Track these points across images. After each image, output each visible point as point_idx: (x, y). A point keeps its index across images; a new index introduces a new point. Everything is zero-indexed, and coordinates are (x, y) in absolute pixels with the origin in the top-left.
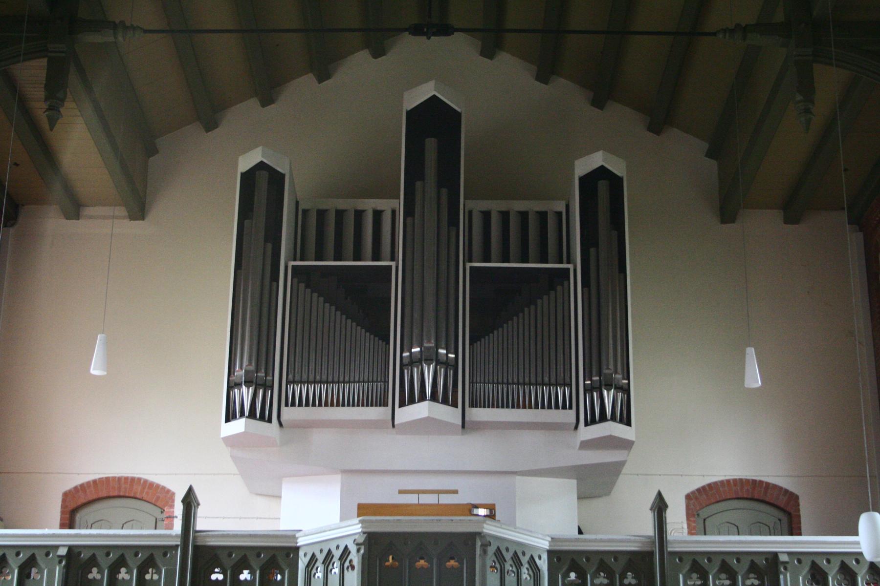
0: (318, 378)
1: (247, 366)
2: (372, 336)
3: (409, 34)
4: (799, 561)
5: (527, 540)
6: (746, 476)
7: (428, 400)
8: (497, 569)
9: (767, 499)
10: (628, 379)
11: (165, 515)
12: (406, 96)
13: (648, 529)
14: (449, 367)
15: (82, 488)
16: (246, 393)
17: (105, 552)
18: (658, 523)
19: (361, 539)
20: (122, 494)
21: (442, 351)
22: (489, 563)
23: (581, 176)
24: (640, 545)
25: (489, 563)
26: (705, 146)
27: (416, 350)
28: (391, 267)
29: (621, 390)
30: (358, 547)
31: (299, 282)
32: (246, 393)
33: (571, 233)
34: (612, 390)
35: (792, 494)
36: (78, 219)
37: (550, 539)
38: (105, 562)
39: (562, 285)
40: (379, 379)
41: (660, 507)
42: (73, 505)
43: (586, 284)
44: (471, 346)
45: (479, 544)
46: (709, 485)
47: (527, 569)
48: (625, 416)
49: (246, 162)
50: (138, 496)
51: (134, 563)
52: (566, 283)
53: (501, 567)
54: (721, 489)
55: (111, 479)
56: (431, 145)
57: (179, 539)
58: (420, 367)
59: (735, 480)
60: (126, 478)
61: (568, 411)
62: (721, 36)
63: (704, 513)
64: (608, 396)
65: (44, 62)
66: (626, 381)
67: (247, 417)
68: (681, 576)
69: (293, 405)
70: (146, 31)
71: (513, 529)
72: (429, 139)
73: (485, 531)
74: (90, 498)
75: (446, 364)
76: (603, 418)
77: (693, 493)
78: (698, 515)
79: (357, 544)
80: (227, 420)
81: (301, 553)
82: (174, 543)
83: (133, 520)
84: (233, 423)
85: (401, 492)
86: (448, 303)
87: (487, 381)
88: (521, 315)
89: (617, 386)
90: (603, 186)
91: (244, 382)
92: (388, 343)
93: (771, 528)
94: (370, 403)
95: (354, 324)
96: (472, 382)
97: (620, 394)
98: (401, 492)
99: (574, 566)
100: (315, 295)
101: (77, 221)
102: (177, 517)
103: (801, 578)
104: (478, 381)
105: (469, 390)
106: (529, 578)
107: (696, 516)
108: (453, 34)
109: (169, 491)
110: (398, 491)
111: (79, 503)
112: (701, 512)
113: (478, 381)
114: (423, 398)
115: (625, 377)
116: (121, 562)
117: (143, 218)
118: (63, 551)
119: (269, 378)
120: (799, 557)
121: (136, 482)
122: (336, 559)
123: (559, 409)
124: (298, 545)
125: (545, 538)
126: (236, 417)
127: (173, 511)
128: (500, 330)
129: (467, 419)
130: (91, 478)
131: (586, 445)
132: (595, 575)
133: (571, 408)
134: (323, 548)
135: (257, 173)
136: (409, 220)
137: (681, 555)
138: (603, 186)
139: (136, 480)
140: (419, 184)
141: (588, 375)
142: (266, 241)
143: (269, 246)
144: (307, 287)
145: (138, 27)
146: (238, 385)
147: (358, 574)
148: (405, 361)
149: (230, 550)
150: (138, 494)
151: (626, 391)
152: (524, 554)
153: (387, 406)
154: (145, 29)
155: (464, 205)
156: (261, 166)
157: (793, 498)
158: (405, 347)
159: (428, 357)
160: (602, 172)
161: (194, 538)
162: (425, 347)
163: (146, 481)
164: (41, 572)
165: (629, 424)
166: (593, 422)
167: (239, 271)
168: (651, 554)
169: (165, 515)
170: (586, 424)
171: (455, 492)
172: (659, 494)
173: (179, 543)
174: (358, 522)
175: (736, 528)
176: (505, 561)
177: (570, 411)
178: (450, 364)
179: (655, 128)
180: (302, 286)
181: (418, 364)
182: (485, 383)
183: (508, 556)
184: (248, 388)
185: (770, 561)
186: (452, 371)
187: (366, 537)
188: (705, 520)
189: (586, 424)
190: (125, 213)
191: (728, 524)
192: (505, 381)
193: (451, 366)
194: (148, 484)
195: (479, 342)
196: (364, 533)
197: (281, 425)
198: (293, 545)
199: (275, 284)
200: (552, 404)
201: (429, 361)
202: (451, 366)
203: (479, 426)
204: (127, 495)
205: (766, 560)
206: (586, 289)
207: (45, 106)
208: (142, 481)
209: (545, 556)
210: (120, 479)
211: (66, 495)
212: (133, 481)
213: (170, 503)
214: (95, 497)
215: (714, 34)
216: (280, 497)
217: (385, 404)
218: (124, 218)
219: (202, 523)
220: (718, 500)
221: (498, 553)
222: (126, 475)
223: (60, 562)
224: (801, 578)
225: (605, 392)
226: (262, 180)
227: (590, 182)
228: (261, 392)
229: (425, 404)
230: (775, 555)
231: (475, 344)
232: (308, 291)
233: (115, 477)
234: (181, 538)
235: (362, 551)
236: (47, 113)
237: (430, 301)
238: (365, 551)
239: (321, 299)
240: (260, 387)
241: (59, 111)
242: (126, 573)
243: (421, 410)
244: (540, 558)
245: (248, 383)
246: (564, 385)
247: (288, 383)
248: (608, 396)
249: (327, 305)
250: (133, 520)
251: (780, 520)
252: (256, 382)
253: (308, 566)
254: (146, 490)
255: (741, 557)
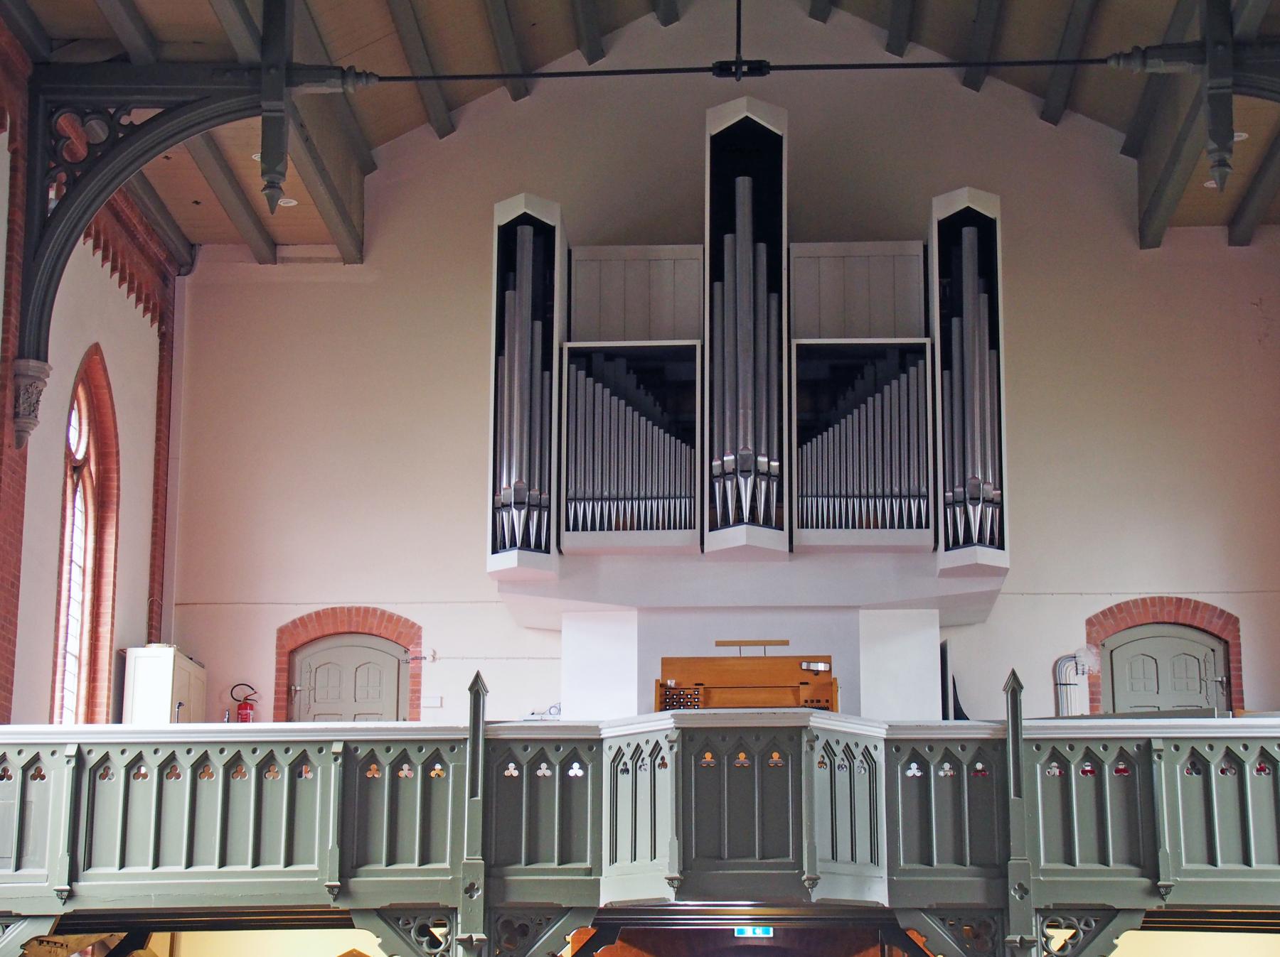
0: (606, 494)
1: (516, 483)
2: (673, 438)
3: (714, 75)
4: (1177, 748)
5: (863, 730)
6: (1168, 593)
7: (746, 523)
8: (826, 765)
9: (1195, 624)
10: (1001, 488)
11: (410, 656)
12: (710, 113)
13: (1001, 712)
14: (772, 478)
15: (302, 622)
16: (518, 516)
17: (385, 747)
18: (1012, 708)
19: (675, 735)
20: (353, 630)
21: (763, 460)
22: (817, 758)
23: (940, 219)
24: (991, 732)
25: (817, 758)
26: (1119, 138)
27: (729, 458)
28: (694, 346)
29: (990, 504)
30: (671, 744)
31: (577, 370)
32: (518, 516)
33: (930, 280)
34: (980, 506)
35: (1230, 616)
36: (276, 264)
37: (887, 727)
38: (386, 759)
39: (916, 365)
40: (683, 494)
41: (1014, 688)
42: (291, 646)
43: (947, 364)
44: (800, 449)
45: (805, 739)
46: (1118, 606)
47: (861, 761)
48: (997, 536)
49: (505, 213)
50: (374, 633)
51: (418, 758)
52: (921, 362)
53: (831, 762)
54: (1134, 611)
55: (338, 611)
56: (743, 185)
57: (468, 733)
58: (735, 480)
59: (1153, 599)
60: (358, 609)
61: (924, 531)
62: (1112, 63)
63: (1111, 642)
64: (975, 513)
65: (257, 122)
66: (999, 492)
67: (519, 549)
68: (1038, 766)
69: (575, 528)
70: (381, 79)
71: (844, 720)
72: (741, 177)
73: (811, 724)
74: (313, 636)
75: (768, 475)
76: (968, 541)
77: (1096, 616)
78: (1103, 645)
79: (669, 742)
80: (494, 551)
81: (606, 746)
82: (462, 737)
83: (370, 663)
84: (502, 556)
85: (719, 644)
86: (768, 318)
87: (820, 494)
88: (863, 406)
89: (986, 499)
90: (969, 235)
91: (514, 503)
92: (693, 446)
93: (1201, 661)
94: (671, 525)
95: (650, 423)
96: (801, 496)
97: (991, 508)
98: (719, 644)
99: (915, 757)
100: (599, 386)
101: (273, 266)
102: (425, 658)
103: (1178, 767)
104: (809, 494)
105: (798, 484)
106: (863, 772)
107: (1101, 647)
108: (769, 73)
109: (413, 625)
110: (714, 644)
111: (300, 642)
112: (1107, 642)
113: (809, 494)
114: (739, 520)
115: (997, 487)
116: (404, 758)
117: (361, 261)
118: (338, 748)
119: (545, 496)
120: (1176, 743)
121: (371, 613)
122: (646, 754)
123: (913, 528)
124: (602, 737)
125: (881, 726)
126: (504, 547)
127: (421, 651)
128: (837, 426)
129: (795, 543)
130: (312, 609)
131: (946, 573)
132: (939, 766)
133: (927, 526)
134: (631, 742)
135: (518, 228)
136: (717, 285)
137: (1038, 743)
138: (969, 235)
139: (371, 611)
140: (728, 238)
141: (950, 484)
142: (534, 318)
143: (538, 325)
144: (588, 375)
145: (371, 74)
146: (506, 506)
147: (671, 772)
148: (716, 471)
149: (526, 743)
150: (375, 629)
151: (1000, 505)
152: (857, 745)
153: (694, 528)
154: (380, 76)
155: (788, 250)
156: (525, 219)
157: (1232, 621)
158: (716, 456)
159: (744, 468)
160: (968, 216)
161: (485, 731)
162: (740, 455)
163: (383, 612)
164: (314, 770)
165: (1001, 547)
166: (956, 544)
167: (500, 357)
168: (1003, 742)
169: (410, 656)
170: (947, 548)
171: (786, 643)
172: (1014, 673)
173: (468, 736)
174: (670, 716)
175: (1154, 661)
176: (836, 755)
177: (927, 530)
178: (773, 474)
179: (1052, 116)
180: (582, 373)
181: (732, 475)
182: (817, 496)
183: (838, 750)
184: (520, 511)
185: (1142, 748)
186: (775, 484)
187: (679, 734)
188: (1112, 651)
189: (947, 548)
190: (337, 254)
191: (1143, 657)
192: (844, 492)
193: (774, 476)
194: (386, 617)
195: (809, 444)
196: (677, 728)
197: (560, 552)
198: (597, 737)
199: (547, 374)
200: (904, 523)
201: (745, 473)
202: (774, 476)
203: (811, 551)
204: (360, 631)
205: (1138, 747)
206: (946, 372)
207: (262, 183)
208: (379, 612)
209: (881, 746)
210: (349, 610)
211: (282, 632)
212: (367, 612)
213: (416, 641)
214: (319, 634)
215: (1104, 61)
216: (560, 631)
217: (692, 527)
218: (336, 260)
219: (493, 711)
220: (1130, 626)
221: (827, 747)
222: (357, 605)
223: (336, 760)
224: (1178, 767)
225: (970, 508)
226: (526, 233)
227: (951, 228)
228: (536, 514)
229: (743, 528)
230: (1149, 741)
231: (805, 447)
232: (590, 380)
233: (344, 608)
234: (470, 731)
235: (675, 750)
236: (267, 191)
237: (746, 395)
238: (678, 749)
239: (607, 391)
240: (533, 508)
241: (281, 188)
242: (409, 770)
243: (737, 535)
244: (876, 747)
245: (519, 504)
246: (919, 496)
247: (567, 500)
248: (975, 513)
249: (615, 399)
250: (370, 663)
251: (1213, 650)
252: (529, 502)
253: (613, 761)
254: (384, 623)
255: (1108, 743)
